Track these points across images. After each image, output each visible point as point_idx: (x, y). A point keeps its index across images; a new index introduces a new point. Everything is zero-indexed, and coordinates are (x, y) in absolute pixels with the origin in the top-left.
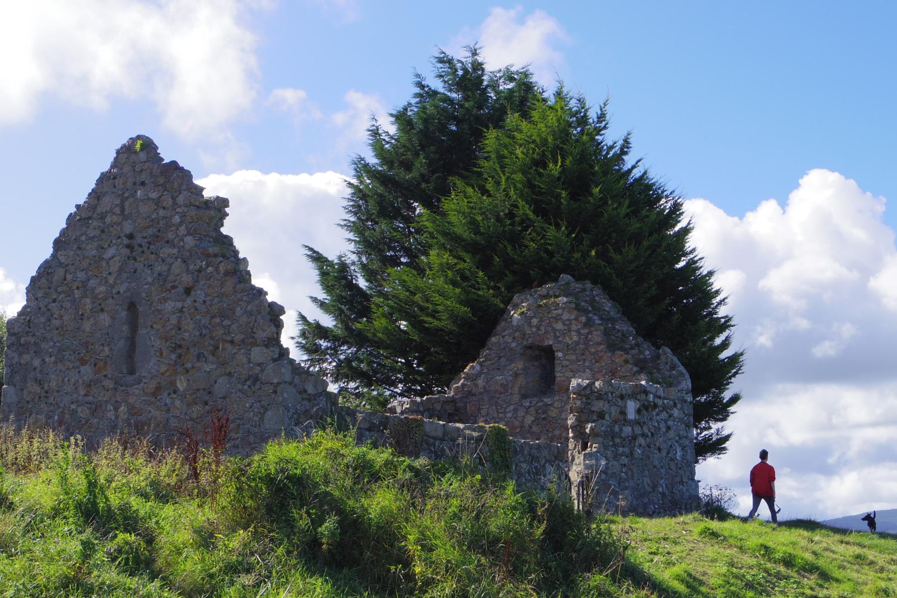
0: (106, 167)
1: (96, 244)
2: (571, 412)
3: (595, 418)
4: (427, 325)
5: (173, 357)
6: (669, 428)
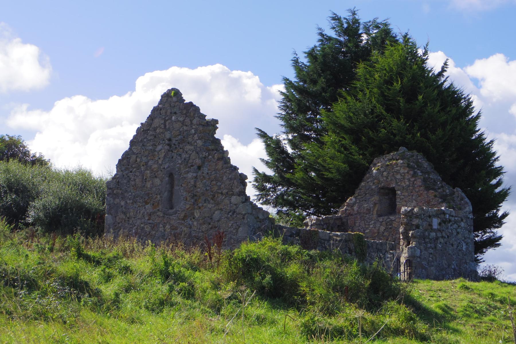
1: (151, 143)
2: (402, 225)
3: (414, 228)
4: (325, 176)
5: (193, 200)
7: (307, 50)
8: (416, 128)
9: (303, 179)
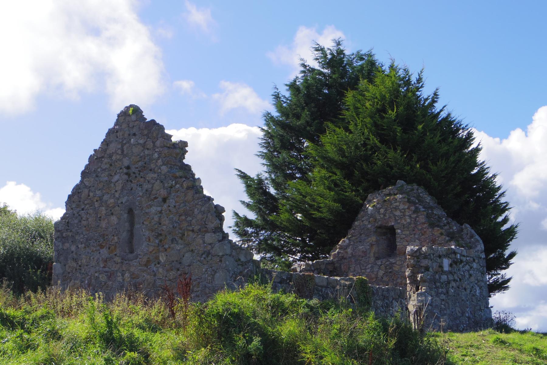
0: (111, 125)
1: (107, 173)
2: (408, 267)
3: (423, 270)
5: (157, 241)
6: (470, 275)
7: (288, 83)
8: (415, 158)
9: (288, 220)
